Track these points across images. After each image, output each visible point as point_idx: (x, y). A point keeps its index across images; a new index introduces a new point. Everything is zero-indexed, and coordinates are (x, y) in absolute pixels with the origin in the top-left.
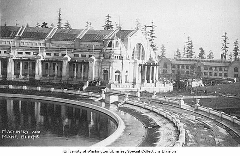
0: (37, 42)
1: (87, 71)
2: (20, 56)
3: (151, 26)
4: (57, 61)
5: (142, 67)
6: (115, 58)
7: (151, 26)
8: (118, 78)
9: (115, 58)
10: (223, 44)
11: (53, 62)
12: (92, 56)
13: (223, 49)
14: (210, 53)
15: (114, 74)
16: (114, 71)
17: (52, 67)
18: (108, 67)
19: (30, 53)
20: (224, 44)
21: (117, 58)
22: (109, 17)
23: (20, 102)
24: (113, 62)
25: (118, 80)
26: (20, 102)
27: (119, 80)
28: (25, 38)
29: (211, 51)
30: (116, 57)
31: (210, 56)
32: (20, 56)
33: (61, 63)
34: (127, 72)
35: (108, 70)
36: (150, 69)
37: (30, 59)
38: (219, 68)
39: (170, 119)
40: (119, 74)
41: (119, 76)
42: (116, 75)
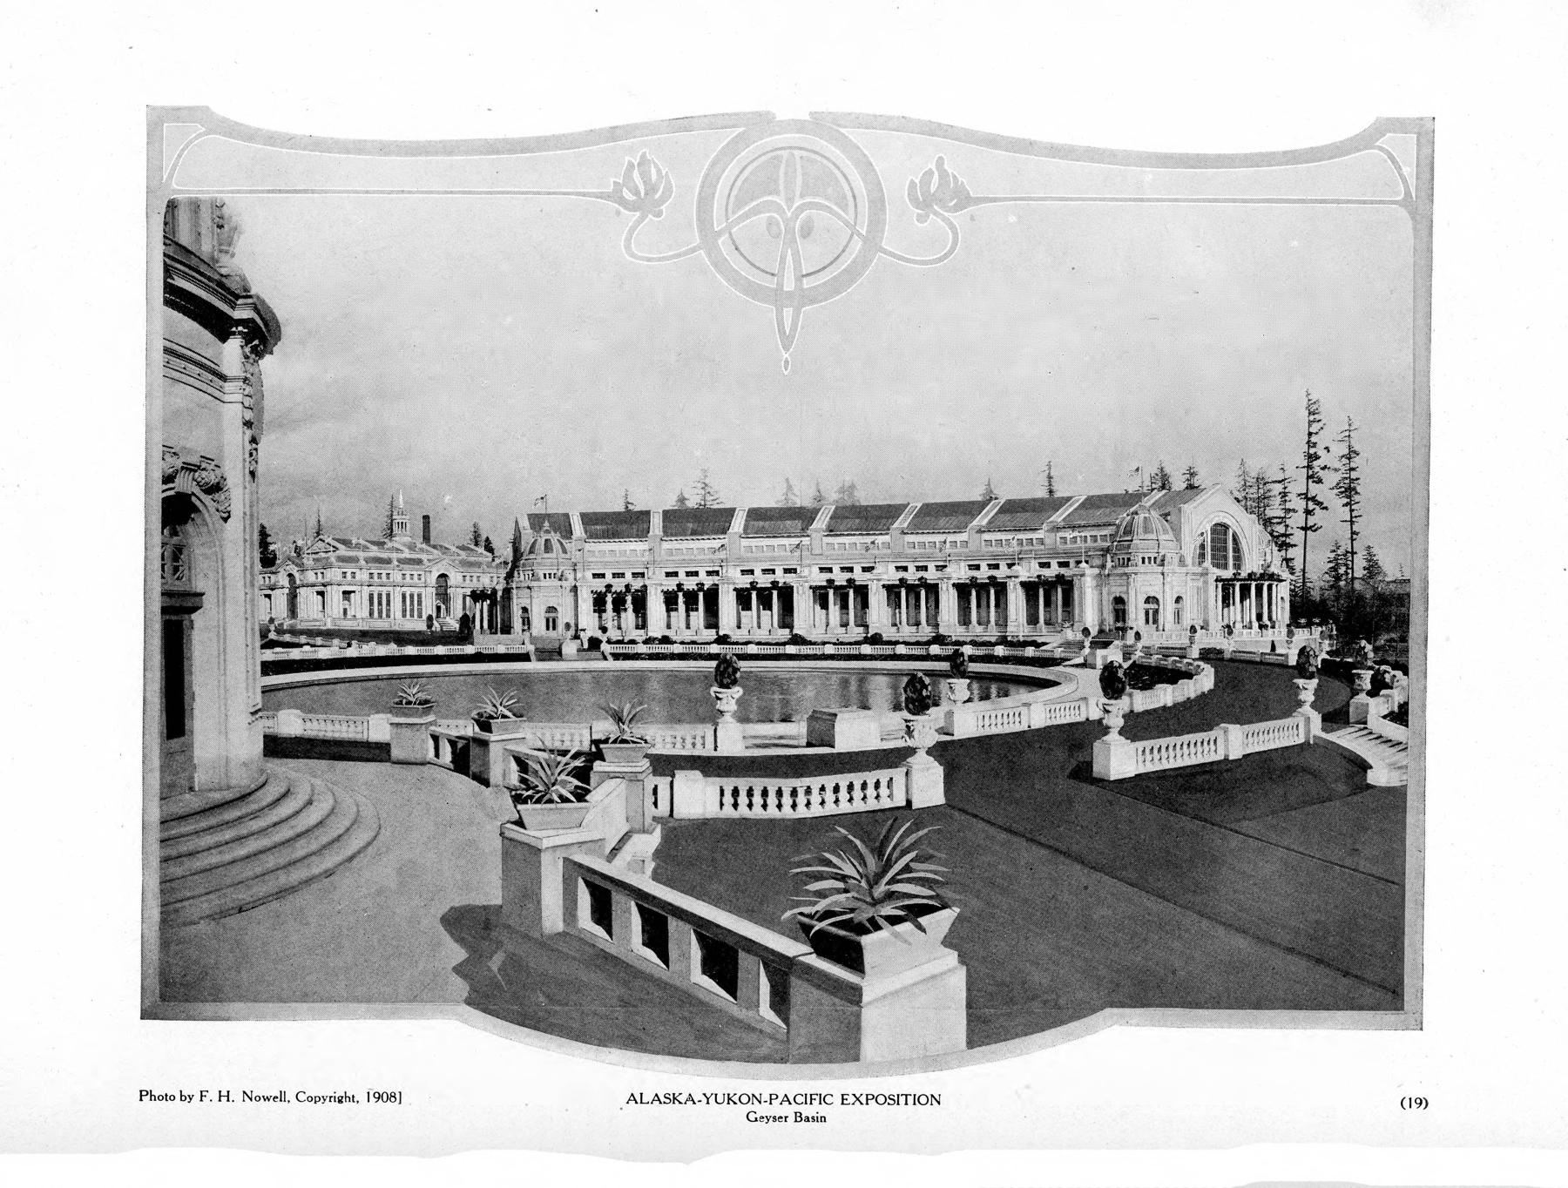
1: (1002, 606)
3: (1280, 482)
4: (923, 583)
6: (1143, 562)
7: (1280, 482)
8: (1152, 617)
9: (1143, 562)
11: (1049, 586)
12: (1081, 562)
15: (1142, 606)
16: (1142, 599)
17: (912, 601)
18: (529, 601)
19: (1049, 563)
21: (1150, 563)
24: (1136, 574)
27: (1155, 621)
28: (700, 537)
30: (1147, 560)
34: (1178, 599)
35: (1160, 597)
36: (1262, 589)
40: (1154, 606)
41: (1156, 612)
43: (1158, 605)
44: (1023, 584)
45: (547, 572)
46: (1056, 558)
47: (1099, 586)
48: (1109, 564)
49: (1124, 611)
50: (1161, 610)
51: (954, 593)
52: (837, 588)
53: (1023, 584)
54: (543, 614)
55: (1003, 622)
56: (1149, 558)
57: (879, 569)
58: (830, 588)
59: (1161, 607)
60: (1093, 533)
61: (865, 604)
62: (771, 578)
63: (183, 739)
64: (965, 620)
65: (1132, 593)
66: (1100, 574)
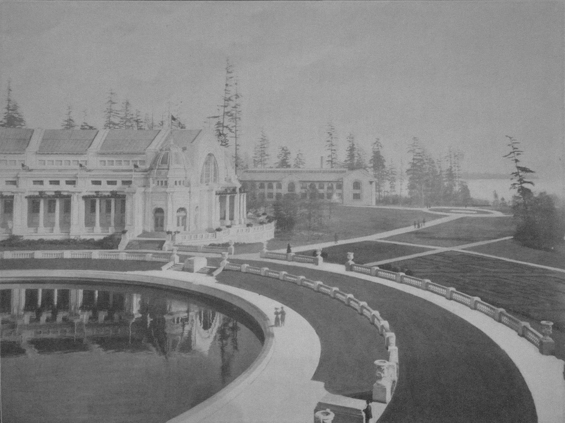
0: (114, 159)
2: (40, 188)
4: (58, 194)
5: (222, 195)
8: (183, 221)
10: (327, 140)
13: (327, 147)
14: (298, 155)
19: (116, 181)
20: (329, 139)
22: (112, 94)
23: (97, 292)
24: (173, 192)
25: (182, 225)
26: (97, 292)
29: (299, 151)
31: (298, 160)
32: (40, 188)
33: (67, 200)
35: (164, 208)
37: (60, 195)
38: (268, 183)
39: (345, 301)
41: (185, 217)
42: (178, 218)
43: (186, 213)
44: (85, 198)
45: (178, 180)
46: (106, 178)
47: (145, 200)
48: (152, 185)
49: (162, 220)
50: (188, 216)
51: (82, 203)
52: (102, 197)
53: (85, 198)
54: (176, 214)
55: (66, 223)
56: (162, 182)
57: (80, 182)
58: (42, 197)
59: (188, 214)
60: (111, 159)
61: (67, 209)
62: (56, 188)
63: (395, 344)
64: (90, 223)
65: (170, 206)
66: (145, 193)
